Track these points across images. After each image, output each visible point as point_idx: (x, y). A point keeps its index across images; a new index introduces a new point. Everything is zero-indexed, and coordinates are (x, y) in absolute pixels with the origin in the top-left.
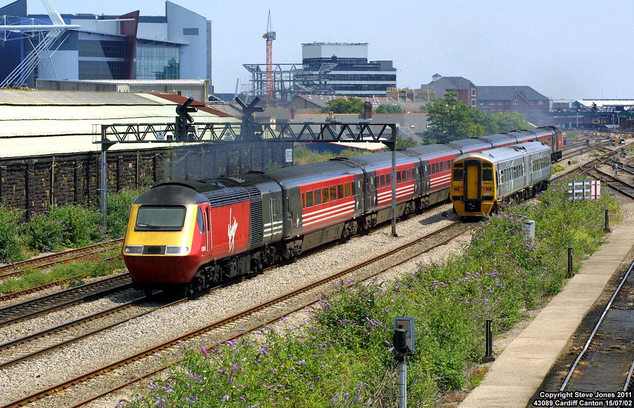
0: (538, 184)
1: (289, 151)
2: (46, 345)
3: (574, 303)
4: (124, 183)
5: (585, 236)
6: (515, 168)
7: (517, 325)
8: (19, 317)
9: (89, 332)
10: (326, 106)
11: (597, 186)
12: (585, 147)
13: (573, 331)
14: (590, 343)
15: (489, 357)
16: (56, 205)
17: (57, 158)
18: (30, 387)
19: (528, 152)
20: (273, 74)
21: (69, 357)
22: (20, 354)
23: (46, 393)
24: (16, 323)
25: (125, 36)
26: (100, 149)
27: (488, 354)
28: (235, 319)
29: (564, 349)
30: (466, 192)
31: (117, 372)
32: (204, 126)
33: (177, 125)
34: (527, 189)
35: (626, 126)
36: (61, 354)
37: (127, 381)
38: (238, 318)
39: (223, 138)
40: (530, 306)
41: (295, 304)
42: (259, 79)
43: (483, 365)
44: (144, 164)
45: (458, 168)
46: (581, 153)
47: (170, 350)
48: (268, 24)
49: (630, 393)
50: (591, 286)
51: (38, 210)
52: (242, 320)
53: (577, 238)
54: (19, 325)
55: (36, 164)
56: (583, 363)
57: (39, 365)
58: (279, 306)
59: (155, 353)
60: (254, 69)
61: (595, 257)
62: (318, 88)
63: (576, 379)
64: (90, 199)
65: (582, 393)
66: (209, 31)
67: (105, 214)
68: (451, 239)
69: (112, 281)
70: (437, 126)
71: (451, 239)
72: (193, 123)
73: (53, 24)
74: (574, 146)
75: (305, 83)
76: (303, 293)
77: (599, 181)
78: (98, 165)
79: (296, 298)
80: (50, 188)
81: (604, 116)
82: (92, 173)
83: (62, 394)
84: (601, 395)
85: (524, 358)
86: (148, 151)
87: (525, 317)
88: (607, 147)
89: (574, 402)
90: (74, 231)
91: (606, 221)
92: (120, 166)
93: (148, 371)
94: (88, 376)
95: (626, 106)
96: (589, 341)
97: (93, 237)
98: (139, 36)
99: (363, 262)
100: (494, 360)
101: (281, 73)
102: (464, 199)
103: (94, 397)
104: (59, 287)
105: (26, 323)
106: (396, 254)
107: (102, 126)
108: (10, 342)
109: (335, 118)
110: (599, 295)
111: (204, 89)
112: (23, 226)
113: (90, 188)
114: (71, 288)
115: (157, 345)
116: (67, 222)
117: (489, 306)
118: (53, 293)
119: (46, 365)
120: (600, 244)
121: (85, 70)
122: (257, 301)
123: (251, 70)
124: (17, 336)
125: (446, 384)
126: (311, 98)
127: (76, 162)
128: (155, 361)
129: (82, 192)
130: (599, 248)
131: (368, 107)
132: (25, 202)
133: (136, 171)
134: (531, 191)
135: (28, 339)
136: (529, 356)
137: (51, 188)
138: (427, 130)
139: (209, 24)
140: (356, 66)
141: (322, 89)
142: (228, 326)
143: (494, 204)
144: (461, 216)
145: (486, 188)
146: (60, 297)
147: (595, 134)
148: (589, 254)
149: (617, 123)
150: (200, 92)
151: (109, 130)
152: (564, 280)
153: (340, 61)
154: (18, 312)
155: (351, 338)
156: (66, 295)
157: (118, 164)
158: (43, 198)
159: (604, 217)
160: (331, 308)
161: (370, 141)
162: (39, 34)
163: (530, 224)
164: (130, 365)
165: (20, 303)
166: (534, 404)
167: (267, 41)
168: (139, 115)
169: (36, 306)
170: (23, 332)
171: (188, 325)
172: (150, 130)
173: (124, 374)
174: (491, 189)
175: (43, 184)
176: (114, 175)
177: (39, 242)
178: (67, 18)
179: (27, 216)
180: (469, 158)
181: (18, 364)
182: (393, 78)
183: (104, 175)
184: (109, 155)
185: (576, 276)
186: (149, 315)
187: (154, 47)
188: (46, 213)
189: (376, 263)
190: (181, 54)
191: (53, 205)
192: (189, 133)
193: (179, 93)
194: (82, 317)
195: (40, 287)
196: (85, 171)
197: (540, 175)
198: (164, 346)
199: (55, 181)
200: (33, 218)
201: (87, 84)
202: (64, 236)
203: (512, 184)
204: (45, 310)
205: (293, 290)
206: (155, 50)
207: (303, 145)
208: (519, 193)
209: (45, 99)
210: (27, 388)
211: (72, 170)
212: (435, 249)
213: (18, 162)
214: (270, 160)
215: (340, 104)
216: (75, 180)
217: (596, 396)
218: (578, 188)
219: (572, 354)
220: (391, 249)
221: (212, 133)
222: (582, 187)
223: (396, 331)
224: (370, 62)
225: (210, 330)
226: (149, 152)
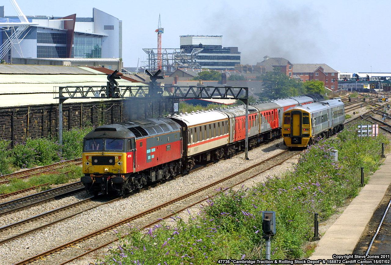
0: (336, 127)
1: (176, 105)
2: (31, 228)
3: (367, 203)
4: (73, 124)
5: (370, 160)
6: (323, 116)
7: (331, 217)
8: (11, 210)
9: (57, 220)
10: (197, 76)
11: (376, 128)
12: (362, 103)
13: (368, 221)
14: (380, 229)
15: (316, 237)
16: (30, 138)
17: (31, 108)
18: (24, 255)
19: (330, 106)
20: (162, 55)
21: (47, 236)
22: (15, 233)
23: (35, 259)
24: (10, 213)
25: (67, 30)
26: (58, 102)
27: (316, 236)
28: (151, 212)
29: (364, 233)
30: (292, 131)
31: (78, 246)
32: (125, 88)
33: (108, 87)
34: (330, 130)
35: (387, 89)
36: (42, 234)
37: (85, 252)
38: (153, 212)
39: (137, 96)
40: (339, 204)
41: (188, 202)
42: (153, 58)
43: (312, 243)
44: (86, 112)
45: (287, 116)
46: (361, 107)
47: (111, 232)
48: (159, 23)
49: (389, 256)
50: (377, 192)
51: (19, 141)
52: (155, 212)
53: (365, 161)
54: (12, 215)
55: (18, 111)
56: (377, 241)
57: (28, 241)
58: (178, 204)
59: (101, 233)
60: (150, 52)
61: (377, 173)
62: (190, 64)
63: (373, 251)
64: (52, 134)
65: (359, 255)
66: (120, 27)
67: (61, 144)
68: (283, 161)
69: (68, 187)
70: (268, 89)
71: (283, 161)
72: (118, 86)
73: (21, 22)
74: (355, 102)
75: (182, 61)
76: (192, 196)
77: (378, 125)
78: (56, 112)
79: (188, 198)
80: (26, 127)
81: (374, 83)
82: (53, 117)
83: (45, 259)
84: (371, 257)
85: (339, 238)
86: (88, 104)
87: (336, 212)
88: (377, 103)
89: (354, 261)
90: (42, 155)
91: (382, 151)
92: (71, 113)
93: (99, 245)
94: (60, 248)
95: (388, 77)
96: (379, 228)
97: (54, 159)
98: (76, 30)
99: (229, 176)
100: (319, 239)
101: (166, 54)
102: (291, 136)
103: (65, 262)
104: (35, 191)
105: (17, 214)
106: (250, 171)
107: (60, 87)
108: (7, 226)
109: (203, 83)
110: (382, 198)
111: (119, 65)
112: (10, 151)
113: (51, 128)
114: (43, 191)
115: (102, 228)
116: (38, 149)
117: (314, 205)
118: (32, 195)
119: (32, 241)
120: (380, 165)
121: (41, 51)
122: (163, 201)
123: (148, 52)
124: (12, 222)
125: (290, 254)
126: (187, 70)
127: (43, 111)
128: (102, 239)
129: (46, 130)
130: (379, 167)
131: (224, 76)
132: (11, 136)
133: (80, 117)
134: (332, 131)
135: (19, 224)
136: (342, 237)
137: (27, 127)
138: (262, 92)
139: (120, 23)
140: (214, 50)
141: (193, 65)
142: (147, 217)
143: (310, 139)
144: (289, 147)
145: (305, 129)
146: (36, 197)
147: (368, 94)
148: (372, 171)
149: (381, 88)
150: (117, 66)
151: (64, 90)
152: (359, 189)
153: (204, 47)
154: (10, 206)
155: (228, 225)
156: (40, 196)
157: (69, 112)
158: (22, 134)
159: (381, 148)
160: (215, 205)
161: (231, 98)
162: (12, 28)
163: (335, 152)
164: (86, 241)
165: (11, 201)
166: (218, 262)
167: (158, 34)
168: (85, 82)
169: (21, 203)
170: (15, 219)
171: (121, 216)
172: (90, 90)
173: (83, 247)
174: (308, 129)
175: (22, 125)
176: (67, 119)
177: (20, 161)
178: (30, 18)
179: (12, 145)
180: (294, 110)
181: (14, 240)
182: (238, 58)
183: (61, 119)
184: (64, 106)
185: (366, 186)
186: (95, 209)
187: (85, 37)
188: (24, 143)
189: (237, 176)
190: (103, 42)
191: (28, 138)
192: (116, 92)
193: (103, 66)
194: (52, 210)
195: (23, 191)
196: (48, 116)
197: (338, 121)
198: (107, 229)
199: (30, 122)
200: (16, 146)
201: (44, 60)
202: (35, 158)
203: (321, 126)
204: (28, 206)
205: (185, 193)
206: (86, 39)
207: (183, 101)
208: (325, 132)
209: (22, 70)
210: (22, 256)
211: (40, 116)
212: (274, 168)
213: (6, 110)
214: (165, 110)
215: (205, 75)
216: (42, 122)
217: (367, 258)
218: (364, 129)
219: (369, 236)
220: (246, 168)
221: (130, 92)
222: (366, 129)
223: (264, 220)
224: (224, 48)
225: (135, 219)
226: (88, 105)
